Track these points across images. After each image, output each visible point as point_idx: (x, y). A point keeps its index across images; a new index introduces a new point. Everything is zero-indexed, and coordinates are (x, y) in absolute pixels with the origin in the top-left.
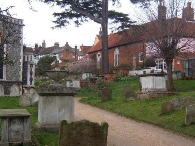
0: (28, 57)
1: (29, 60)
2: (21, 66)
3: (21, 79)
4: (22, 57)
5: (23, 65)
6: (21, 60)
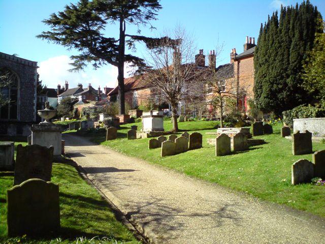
0: (42, 99)
6: (35, 101)
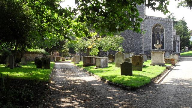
0: (176, 38)
1: (177, 39)
2: (173, 43)
3: (173, 49)
4: (173, 38)
5: (174, 42)
6: (173, 40)
